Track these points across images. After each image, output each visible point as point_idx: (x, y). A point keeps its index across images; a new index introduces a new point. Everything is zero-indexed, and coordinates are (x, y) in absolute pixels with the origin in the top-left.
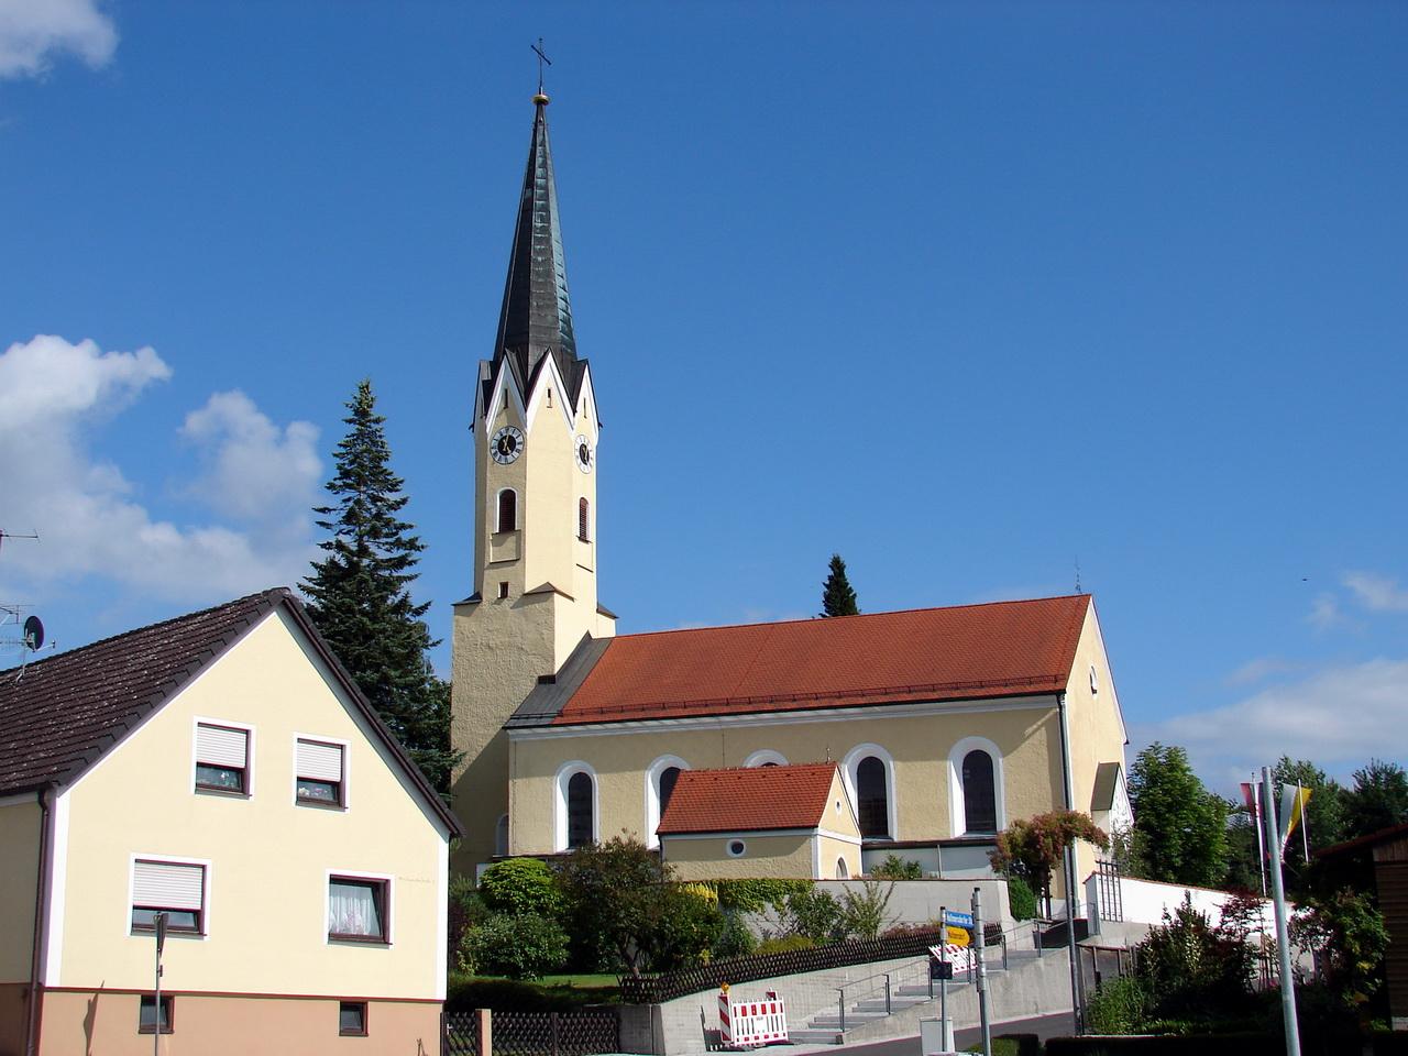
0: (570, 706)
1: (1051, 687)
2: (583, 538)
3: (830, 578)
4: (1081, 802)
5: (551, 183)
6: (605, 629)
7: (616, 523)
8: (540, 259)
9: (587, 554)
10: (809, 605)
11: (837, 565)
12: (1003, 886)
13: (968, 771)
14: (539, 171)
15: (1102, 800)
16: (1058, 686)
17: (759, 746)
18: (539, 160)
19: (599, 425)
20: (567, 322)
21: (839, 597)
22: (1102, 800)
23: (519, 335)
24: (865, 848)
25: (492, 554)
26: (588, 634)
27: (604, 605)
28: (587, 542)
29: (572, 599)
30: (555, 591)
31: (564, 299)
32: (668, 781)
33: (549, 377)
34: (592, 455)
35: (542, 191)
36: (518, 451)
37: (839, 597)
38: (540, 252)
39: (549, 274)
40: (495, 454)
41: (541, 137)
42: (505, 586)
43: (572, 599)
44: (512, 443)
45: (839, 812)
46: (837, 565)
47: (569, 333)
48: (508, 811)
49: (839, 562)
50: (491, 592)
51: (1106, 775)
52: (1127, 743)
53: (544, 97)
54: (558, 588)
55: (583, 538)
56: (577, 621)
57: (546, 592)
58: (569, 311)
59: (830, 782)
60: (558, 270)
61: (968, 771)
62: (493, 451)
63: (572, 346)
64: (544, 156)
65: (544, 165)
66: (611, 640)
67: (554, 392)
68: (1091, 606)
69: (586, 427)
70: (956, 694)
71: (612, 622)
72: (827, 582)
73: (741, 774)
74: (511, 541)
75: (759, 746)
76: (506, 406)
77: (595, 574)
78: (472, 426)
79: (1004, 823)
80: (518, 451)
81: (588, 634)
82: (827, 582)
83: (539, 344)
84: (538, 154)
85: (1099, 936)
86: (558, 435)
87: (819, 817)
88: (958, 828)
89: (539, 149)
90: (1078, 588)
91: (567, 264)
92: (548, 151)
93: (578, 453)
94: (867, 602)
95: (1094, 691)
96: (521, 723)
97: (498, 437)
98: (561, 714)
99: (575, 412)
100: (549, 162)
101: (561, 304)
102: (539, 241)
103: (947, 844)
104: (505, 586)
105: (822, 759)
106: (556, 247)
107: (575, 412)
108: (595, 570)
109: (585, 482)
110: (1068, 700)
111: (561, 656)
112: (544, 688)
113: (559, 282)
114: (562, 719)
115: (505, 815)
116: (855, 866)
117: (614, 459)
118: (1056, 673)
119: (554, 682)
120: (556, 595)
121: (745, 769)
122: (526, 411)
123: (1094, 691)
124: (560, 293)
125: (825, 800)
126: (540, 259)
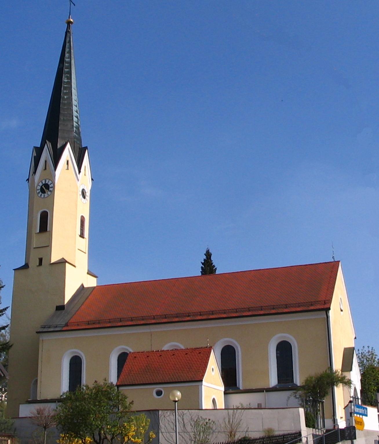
0: (72, 320)
1: (322, 307)
2: (82, 236)
3: (205, 260)
4: (337, 365)
5: (73, 62)
6: (91, 282)
7: (100, 230)
8: (66, 97)
9: (84, 244)
10: (195, 270)
11: (208, 255)
12: (302, 411)
13: (279, 352)
14: (67, 55)
15: (347, 366)
16: (326, 306)
17: (171, 339)
18: (67, 50)
19: (92, 179)
20: (78, 128)
21: (208, 267)
22: (347, 366)
23: (55, 133)
24: (225, 393)
25: (35, 243)
26: (82, 285)
27: (90, 270)
28: (83, 238)
29: (75, 266)
30: (66, 262)
31: (77, 117)
32: (123, 358)
33: (68, 154)
34: (88, 194)
35: (68, 65)
36: (51, 191)
37: (208, 267)
38: (66, 94)
39: (70, 104)
40: (39, 193)
41: (69, 39)
42: (41, 260)
43: (75, 266)
44: (47, 186)
45: (213, 373)
46: (208, 255)
47: (79, 133)
48: (37, 377)
49: (209, 252)
50: (34, 263)
51: (348, 354)
52: (355, 338)
53: (72, 20)
54: (68, 261)
55: (82, 236)
56: (77, 278)
57: (63, 262)
58: (79, 123)
59: (209, 357)
60: (75, 103)
61: (279, 352)
62: (38, 191)
63: (80, 140)
64: (70, 48)
65: (70, 52)
66: (94, 288)
67: (70, 162)
68: (340, 267)
69: (85, 179)
70: (273, 311)
71: (95, 279)
72: (203, 262)
73: (161, 354)
74: (44, 235)
75: (171, 339)
76: (46, 169)
77: (87, 254)
78: (28, 180)
79: (298, 380)
80: (51, 191)
81: (82, 285)
82: (203, 262)
83: (63, 138)
84: (67, 46)
85: (356, 440)
86: (72, 185)
87: (203, 376)
88: (273, 381)
89: (67, 44)
90: (333, 257)
91: (79, 105)
92: (72, 46)
93: (81, 193)
94: (221, 267)
95: (342, 311)
96: (45, 330)
97: (41, 184)
98: (67, 325)
99: (80, 172)
100: (72, 51)
101: (75, 119)
102: (65, 88)
103: (269, 390)
104: (41, 260)
105: (204, 346)
106: (74, 91)
107: (80, 172)
108: (87, 252)
109: (84, 208)
110: (331, 313)
111: (68, 297)
112: (59, 312)
113: (75, 108)
114: (67, 328)
115: (36, 378)
116: (221, 405)
117: (98, 197)
118: (324, 299)
119: (64, 309)
120: (67, 264)
121: (163, 351)
122: (55, 170)
123: (342, 311)
124: (75, 114)
125: (206, 367)
126: (66, 97)
